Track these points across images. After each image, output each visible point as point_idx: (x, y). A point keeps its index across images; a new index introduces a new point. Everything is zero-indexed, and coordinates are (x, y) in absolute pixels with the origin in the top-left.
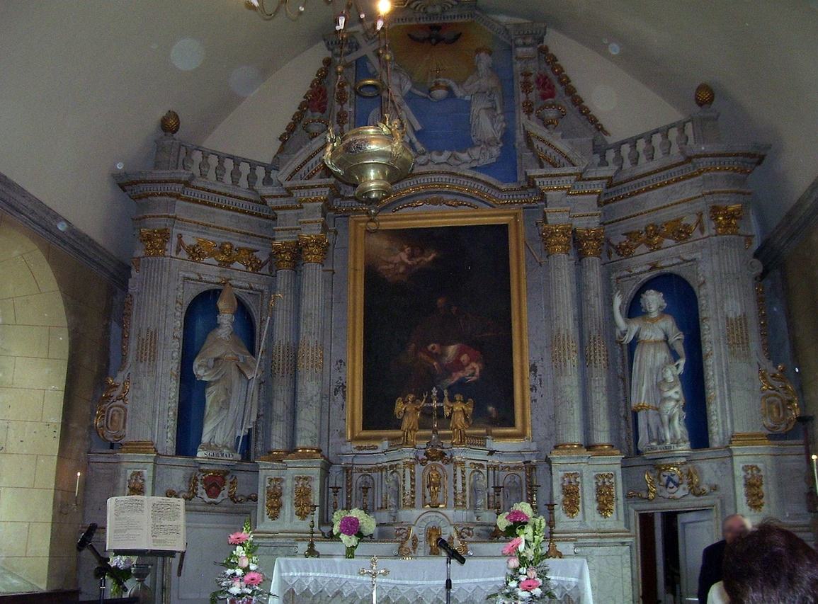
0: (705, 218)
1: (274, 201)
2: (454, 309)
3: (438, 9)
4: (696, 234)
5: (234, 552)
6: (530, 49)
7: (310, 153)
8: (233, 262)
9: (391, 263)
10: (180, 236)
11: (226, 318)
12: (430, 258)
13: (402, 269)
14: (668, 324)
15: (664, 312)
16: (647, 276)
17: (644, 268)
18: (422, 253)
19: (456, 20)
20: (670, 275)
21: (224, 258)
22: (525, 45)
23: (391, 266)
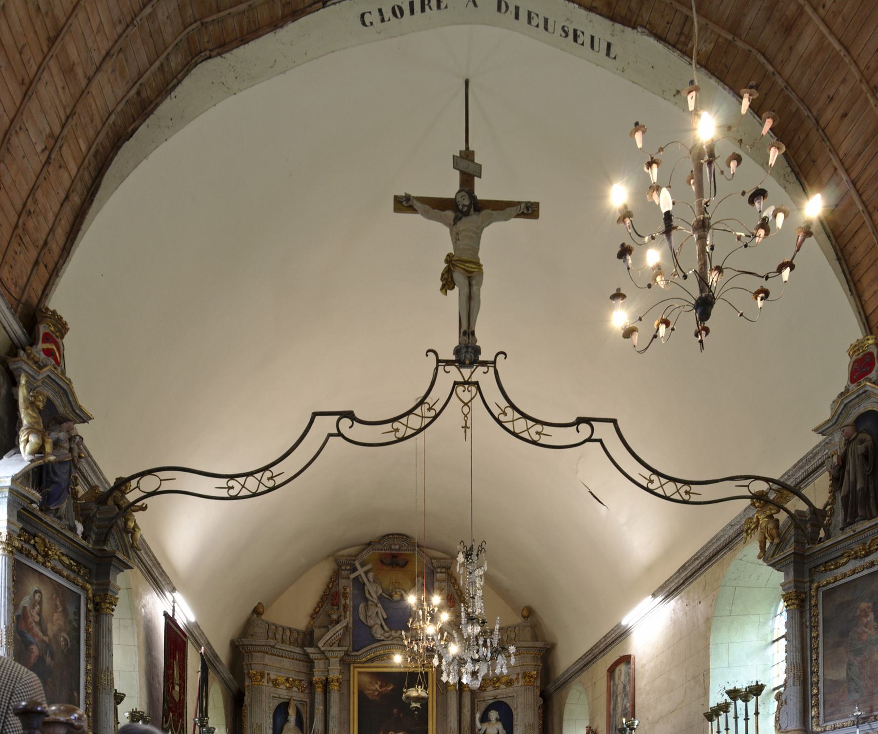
0: (520, 676)
1: (314, 655)
2: (401, 715)
3: (397, 547)
4: (515, 684)
5: (856, 696)
6: (444, 575)
7: (335, 632)
8: (292, 688)
9: (371, 690)
10: (268, 674)
11: (292, 717)
12: (390, 688)
13: (376, 693)
14: (500, 726)
15: (497, 720)
16: (491, 701)
17: (491, 698)
18: (386, 686)
19: (405, 552)
20: (502, 702)
21: (288, 685)
22: (441, 572)
23: (371, 692)
